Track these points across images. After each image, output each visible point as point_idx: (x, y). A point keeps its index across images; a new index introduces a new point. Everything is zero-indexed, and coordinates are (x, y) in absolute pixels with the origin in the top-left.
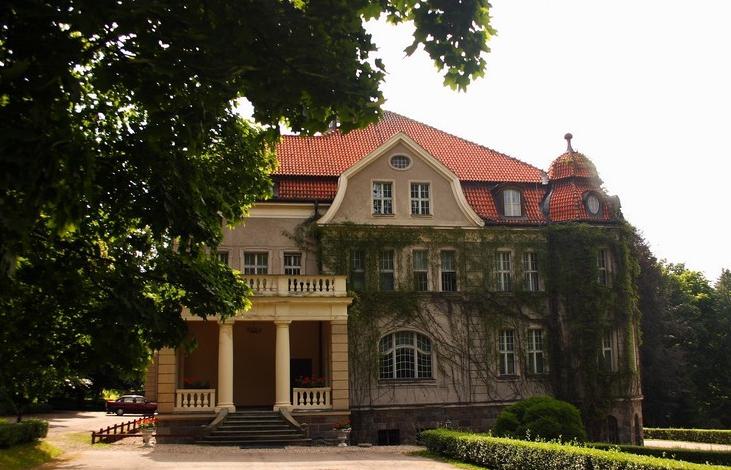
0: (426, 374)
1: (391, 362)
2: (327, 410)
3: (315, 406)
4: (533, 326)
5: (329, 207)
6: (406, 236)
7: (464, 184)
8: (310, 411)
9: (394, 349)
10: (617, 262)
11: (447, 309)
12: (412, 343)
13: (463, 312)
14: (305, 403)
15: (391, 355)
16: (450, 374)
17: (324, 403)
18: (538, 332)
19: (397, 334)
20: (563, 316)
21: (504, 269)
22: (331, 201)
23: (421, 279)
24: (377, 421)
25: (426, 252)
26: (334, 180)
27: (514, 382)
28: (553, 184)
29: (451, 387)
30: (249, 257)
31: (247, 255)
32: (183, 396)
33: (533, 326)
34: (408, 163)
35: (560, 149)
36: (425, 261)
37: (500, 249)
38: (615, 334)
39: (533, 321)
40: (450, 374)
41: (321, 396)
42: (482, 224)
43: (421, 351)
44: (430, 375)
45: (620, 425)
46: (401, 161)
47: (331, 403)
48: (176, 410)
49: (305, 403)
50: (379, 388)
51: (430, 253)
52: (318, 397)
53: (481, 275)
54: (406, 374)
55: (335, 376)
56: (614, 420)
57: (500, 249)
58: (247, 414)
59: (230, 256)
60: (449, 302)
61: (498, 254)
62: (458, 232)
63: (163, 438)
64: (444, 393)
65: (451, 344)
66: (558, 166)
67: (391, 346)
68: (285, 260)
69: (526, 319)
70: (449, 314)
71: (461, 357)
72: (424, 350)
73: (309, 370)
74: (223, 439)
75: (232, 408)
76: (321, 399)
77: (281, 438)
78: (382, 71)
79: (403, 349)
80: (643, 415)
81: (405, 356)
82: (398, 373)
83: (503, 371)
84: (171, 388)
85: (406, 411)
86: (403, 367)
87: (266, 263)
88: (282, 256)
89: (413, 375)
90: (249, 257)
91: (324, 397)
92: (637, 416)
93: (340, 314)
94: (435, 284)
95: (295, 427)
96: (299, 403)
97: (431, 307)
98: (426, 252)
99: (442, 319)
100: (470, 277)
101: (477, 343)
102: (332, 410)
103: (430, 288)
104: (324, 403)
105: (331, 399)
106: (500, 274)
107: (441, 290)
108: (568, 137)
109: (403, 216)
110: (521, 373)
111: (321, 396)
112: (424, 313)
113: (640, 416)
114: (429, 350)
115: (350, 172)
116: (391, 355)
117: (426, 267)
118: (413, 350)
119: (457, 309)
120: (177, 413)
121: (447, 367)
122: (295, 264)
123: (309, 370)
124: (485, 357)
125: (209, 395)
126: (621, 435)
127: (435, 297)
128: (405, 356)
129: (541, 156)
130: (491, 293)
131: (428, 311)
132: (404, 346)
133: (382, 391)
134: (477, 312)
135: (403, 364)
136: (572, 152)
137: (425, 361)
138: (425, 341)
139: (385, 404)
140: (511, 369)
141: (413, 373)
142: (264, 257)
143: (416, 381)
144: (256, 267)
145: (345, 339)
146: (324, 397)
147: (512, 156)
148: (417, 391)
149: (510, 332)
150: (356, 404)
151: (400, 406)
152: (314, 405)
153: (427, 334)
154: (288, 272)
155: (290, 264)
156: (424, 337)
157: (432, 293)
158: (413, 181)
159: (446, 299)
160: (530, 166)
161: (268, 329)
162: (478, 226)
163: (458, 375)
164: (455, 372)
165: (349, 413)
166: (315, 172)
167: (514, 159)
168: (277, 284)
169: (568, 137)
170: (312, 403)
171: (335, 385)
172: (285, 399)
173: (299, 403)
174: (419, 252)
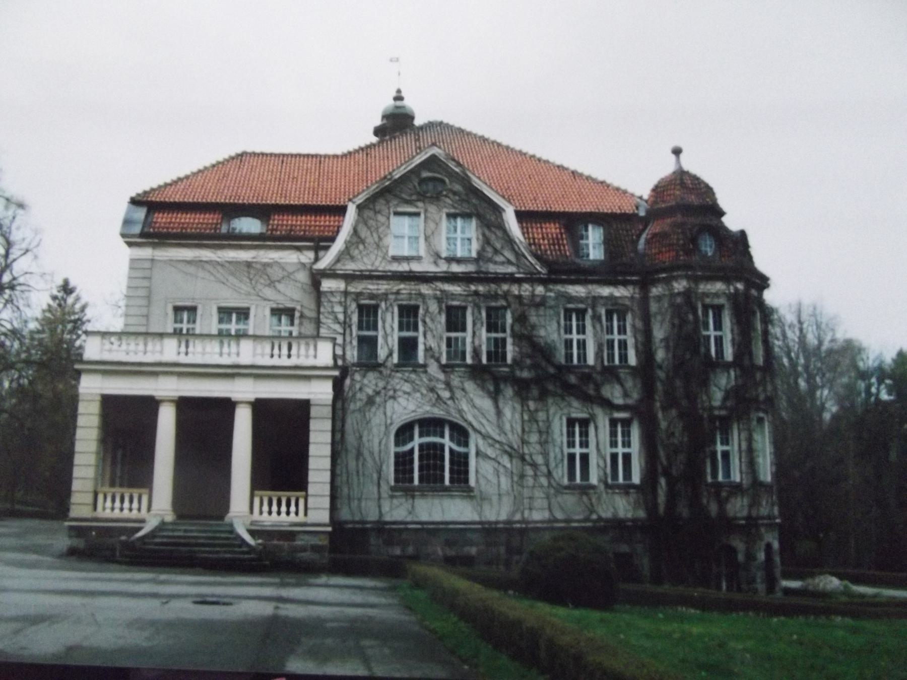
1: (412, 461)
2: (296, 525)
3: (301, 518)
7: (521, 216)
9: (417, 441)
11: (492, 388)
12: (442, 436)
15: (411, 451)
20: (661, 402)
22: (332, 239)
24: (389, 543)
26: (341, 210)
28: (654, 214)
30: (225, 313)
35: (666, 168)
38: (735, 427)
45: (741, 557)
47: (306, 514)
54: (432, 479)
55: (312, 477)
56: (733, 551)
59: (199, 312)
66: (659, 190)
67: (411, 438)
70: (495, 396)
72: (459, 444)
73: (281, 466)
75: (170, 517)
80: (781, 543)
84: (90, 486)
85: (429, 531)
90: (225, 313)
91: (297, 505)
92: (769, 547)
93: (320, 392)
95: (248, 545)
96: (261, 513)
102: (304, 524)
104: (297, 513)
108: (677, 152)
113: (776, 545)
115: (360, 200)
116: (411, 451)
118: (442, 446)
119: (509, 391)
123: (281, 466)
128: (432, 453)
129: (636, 176)
133: (395, 501)
135: (435, 470)
137: (460, 463)
138: (461, 433)
143: (446, 489)
145: (328, 425)
146: (297, 505)
147: (600, 178)
150: (357, 518)
152: (276, 516)
154: (177, 333)
160: (625, 192)
165: (329, 529)
166: (294, 200)
167: (602, 183)
168: (162, 346)
169: (677, 152)
171: (311, 489)
172: (245, 508)
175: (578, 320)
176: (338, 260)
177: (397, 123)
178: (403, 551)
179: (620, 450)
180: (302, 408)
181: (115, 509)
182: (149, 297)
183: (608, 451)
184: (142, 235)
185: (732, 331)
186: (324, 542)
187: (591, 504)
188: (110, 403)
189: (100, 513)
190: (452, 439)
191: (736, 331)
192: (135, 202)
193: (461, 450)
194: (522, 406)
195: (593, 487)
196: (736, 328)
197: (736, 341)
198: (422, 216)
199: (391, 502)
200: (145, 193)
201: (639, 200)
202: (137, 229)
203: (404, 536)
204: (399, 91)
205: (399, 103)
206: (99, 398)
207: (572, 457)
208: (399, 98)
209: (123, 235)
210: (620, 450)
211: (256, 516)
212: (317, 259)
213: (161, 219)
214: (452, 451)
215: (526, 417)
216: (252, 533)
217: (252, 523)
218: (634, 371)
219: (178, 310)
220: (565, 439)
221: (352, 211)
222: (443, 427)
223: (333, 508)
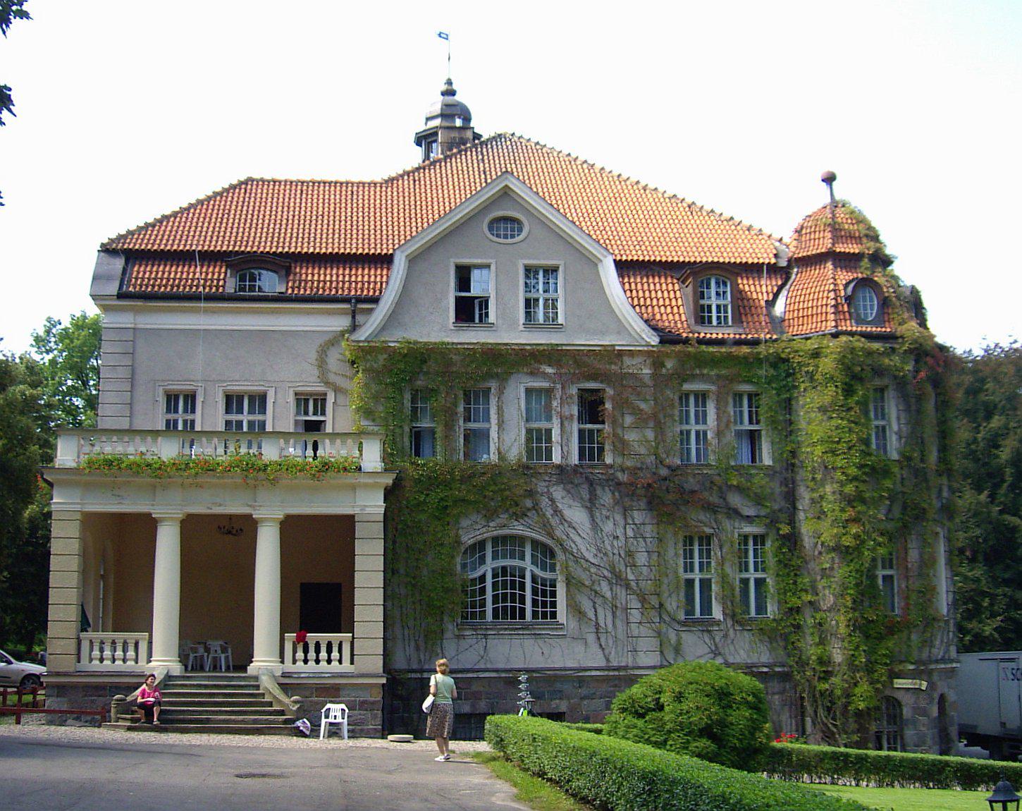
0: (545, 608)
1: (483, 591)
2: (342, 675)
3: (346, 666)
4: (749, 529)
5: (371, 310)
6: (502, 362)
7: (625, 268)
8: (318, 675)
10: (908, 409)
11: (586, 496)
12: (522, 558)
13: (564, 493)
14: (329, 661)
16: (591, 614)
17: (340, 661)
18: (759, 540)
19: (495, 540)
21: (697, 422)
22: (375, 300)
23: (539, 440)
25: (549, 392)
26: (385, 260)
27: (709, 631)
29: (591, 638)
30: (233, 402)
31: (229, 398)
32: (91, 642)
33: (749, 529)
34: (520, 230)
36: (548, 408)
37: (687, 387)
39: (749, 519)
40: (591, 614)
41: (335, 649)
42: (654, 340)
43: (538, 572)
44: (554, 615)
46: (506, 225)
47: (352, 663)
48: (81, 667)
49: (306, 661)
50: (458, 637)
51: (558, 394)
52: (329, 651)
53: (650, 434)
54: (509, 612)
55: (359, 614)
57: (687, 387)
58: (200, 678)
60: (591, 483)
61: (685, 397)
62: (616, 355)
63: (56, 716)
64: (579, 648)
65: (593, 560)
67: (482, 560)
68: (298, 405)
69: (734, 513)
70: (591, 505)
71: (610, 583)
72: (544, 569)
74: (191, 721)
76: (335, 654)
77: (255, 722)
78: (878, 245)
79: (504, 569)
81: (509, 580)
82: (495, 611)
83: (690, 612)
86: (505, 600)
87: (263, 410)
88: (291, 399)
89: (523, 616)
90: (233, 402)
91: (340, 651)
93: (371, 505)
94: (564, 448)
96: (294, 661)
97: (558, 493)
98: (549, 392)
99: (576, 514)
100: (631, 436)
101: (642, 559)
103: (556, 458)
104: (340, 661)
105: (352, 655)
106: (688, 432)
107: (574, 459)
108: (829, 179)
109: (506, 328)
110: (724, 614)
111: (335, 649)
112: (544, 502)
114: (553, 569)
116: (482, 579)
117: (549, 419)
118: (522, 570)
119: (606, 497)
120: (102, 674)
121: (586, 605)
122: (315, 413)
124: (658, 582)
125: (136, 645)
126: (909, 733)
127: (563, 474)
130: (669, 467)
131: (552, 500)
132: (508, 562)
134: (643, 504)
136: (835, 204)
137: (545, 593)
138: (545, 553)
139: (469, 666)
140: (706, 608)
141: (523, 611)
142: (259, 402)
144: (245, 418)
145: (379, 547)
146: (340, 651)
148: (529, 643)
149: (706, 540)
150: (415, 666)
151: (496, 671)
153: (549, 542)
155: (306, 413)
156: (544, 546)
157: (559, 467)
158: (527, 262)
159: (583, 477)
161: (241, 531)
162: (648, 345)
163: (605, 617)
164: (600, 610)
165: (384, 681)
169: (829, 179)
170: (317, 661)
173: (294, 661)
174: (539, 391)
175: (696, 405)
176: (384, 328)
177: (451, 132)
178: (473, 706)
179: (752, 575)
180: (347, 523)
181: (106, 658)
182: (132, 379)
183: (736, 577)
184: (121, 296)
185: (898, 419)
186: (377, 696)
187: (716, 645)
188: (91, 522)
189: (85, 665)
190: (534, 562)
191: (903, 421)
192: (108, 250)
193: (547, 575)
194: (625, 519)
195: (718, 623)
196: (903, 415)
197: (904, 434)
198: (493, 267)
199: (458, 645)
200: (120, 237)
201: (777, 244)
202: (113, 289)
203: (475, 688)
204: (449, 82)
205: (449, 99)
206: (78, 516)
207: (690, 583)
208: (450, 92)
209: (94, 297)
210: (697, 576)
211: (289, 666)
212: (354, 327)
213: (145, 275)
214: (534, 579)
215: (630, 533)
216: (285, 687)
217: (284, 675)
218: (771, 472)
219: (172, 400)
220: (681, 561)
221: (400, 263)
222: (522, 545)
223: (386, 654)
